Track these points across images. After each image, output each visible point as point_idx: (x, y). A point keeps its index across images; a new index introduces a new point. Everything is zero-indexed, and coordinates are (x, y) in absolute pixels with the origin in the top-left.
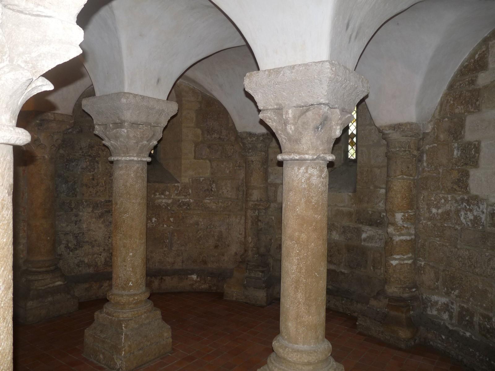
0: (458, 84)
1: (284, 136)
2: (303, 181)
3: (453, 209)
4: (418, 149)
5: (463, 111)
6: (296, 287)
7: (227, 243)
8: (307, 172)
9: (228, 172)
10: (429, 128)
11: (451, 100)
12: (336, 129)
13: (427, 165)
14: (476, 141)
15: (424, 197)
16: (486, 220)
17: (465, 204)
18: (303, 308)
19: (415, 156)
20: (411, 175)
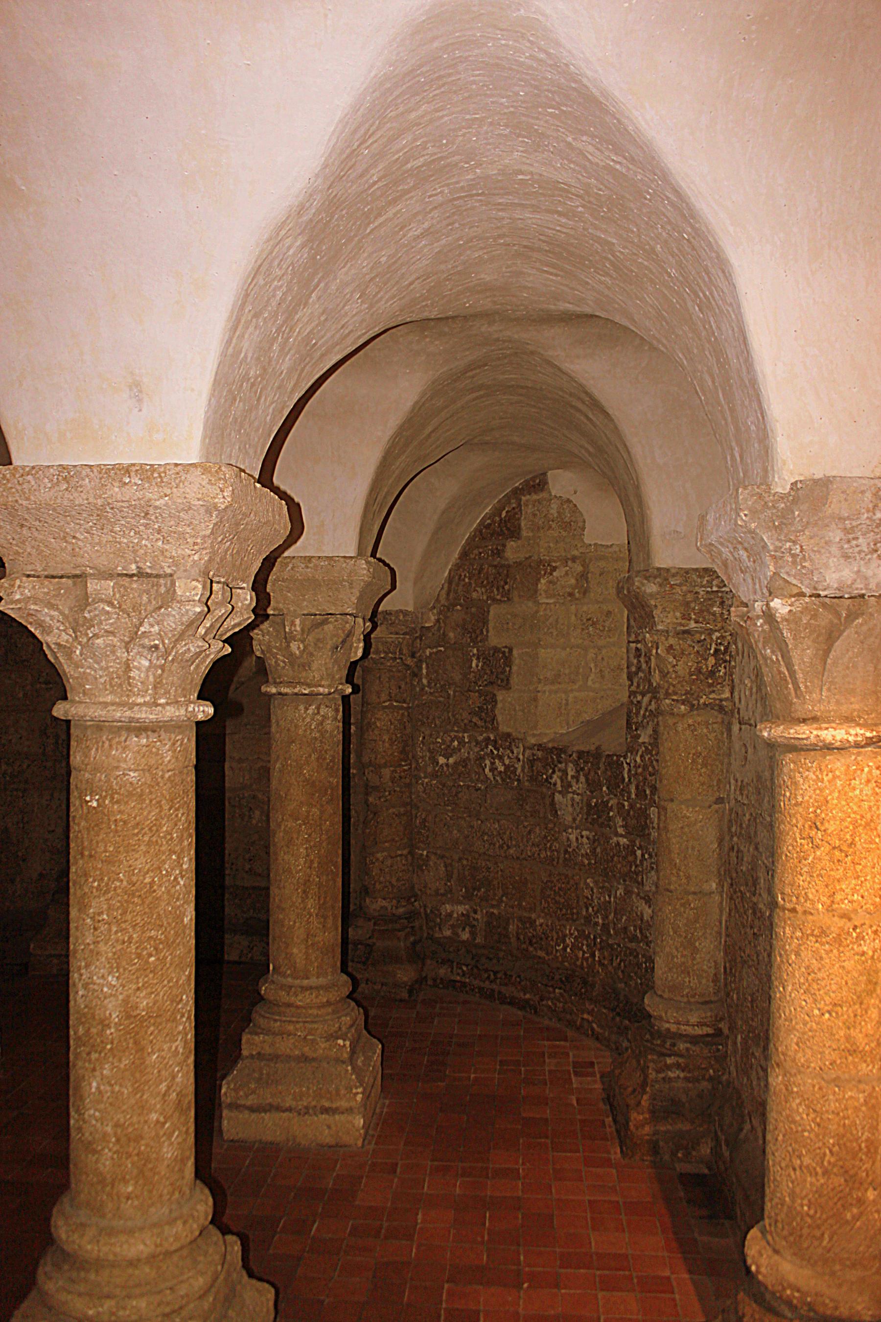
0: (476, 552)
1: (281, 658)
2: (313, 727)
3: (472, 756)
4: (413, 656)
5: (485, 598)
6: (304, 892)
7: (20, 854)
8: (318, 713)
9: (21, 695)
10: (430, 620)
11: (465, 575)
12: (357, 648)
13: (428, 682)
14: (506, 647)
15: (424, 738)
16: (523, 770)
17: (490, 747)
18: (315, 923)
19: (408, 667)
20: (404, 702)
